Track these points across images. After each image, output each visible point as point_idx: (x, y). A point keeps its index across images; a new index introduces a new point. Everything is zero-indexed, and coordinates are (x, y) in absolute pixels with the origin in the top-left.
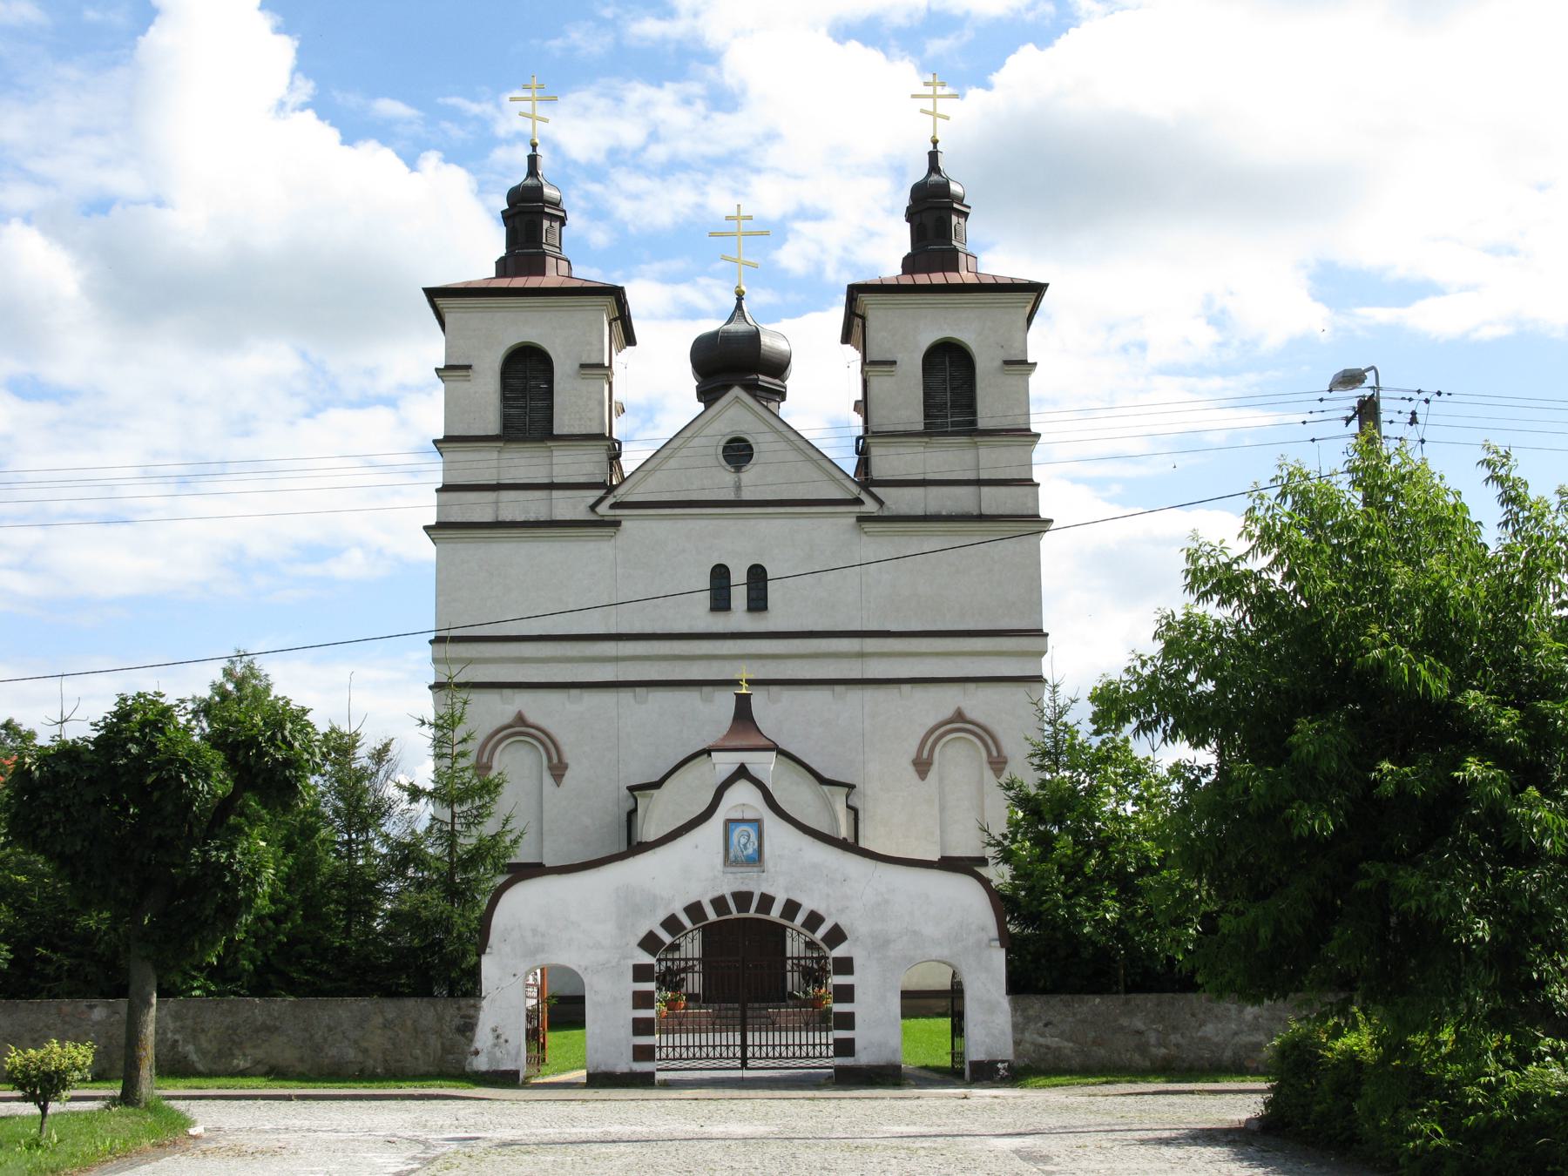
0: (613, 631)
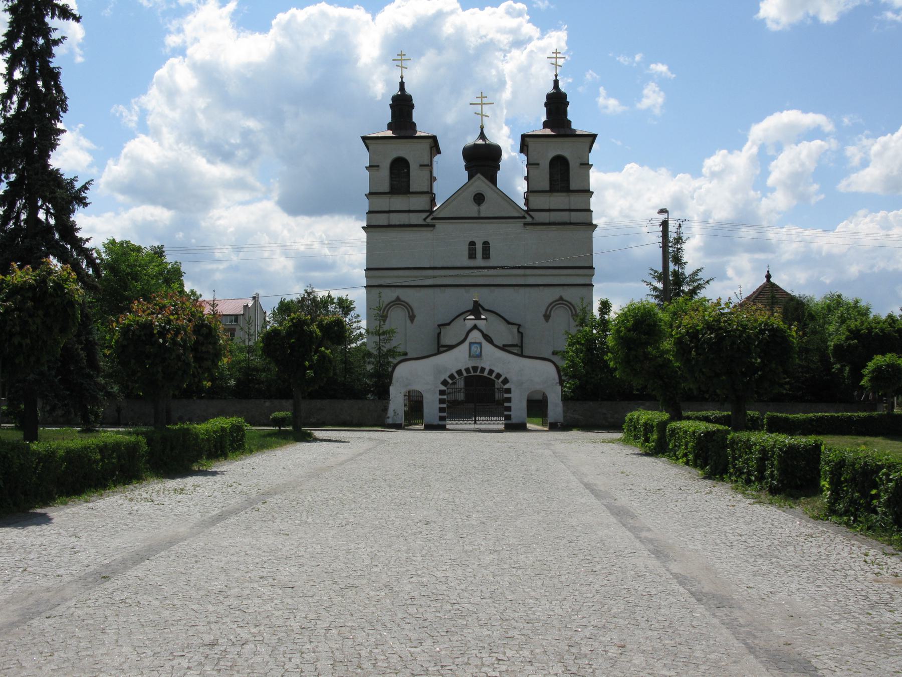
0: (432, 266)
